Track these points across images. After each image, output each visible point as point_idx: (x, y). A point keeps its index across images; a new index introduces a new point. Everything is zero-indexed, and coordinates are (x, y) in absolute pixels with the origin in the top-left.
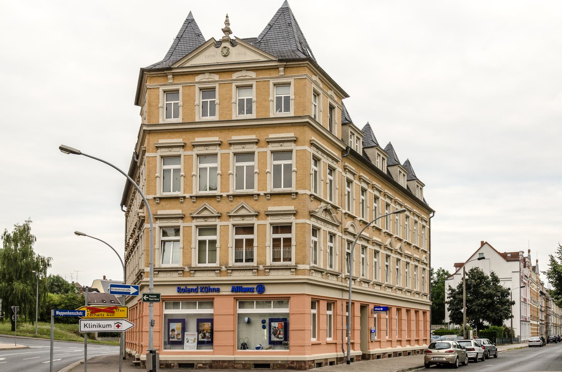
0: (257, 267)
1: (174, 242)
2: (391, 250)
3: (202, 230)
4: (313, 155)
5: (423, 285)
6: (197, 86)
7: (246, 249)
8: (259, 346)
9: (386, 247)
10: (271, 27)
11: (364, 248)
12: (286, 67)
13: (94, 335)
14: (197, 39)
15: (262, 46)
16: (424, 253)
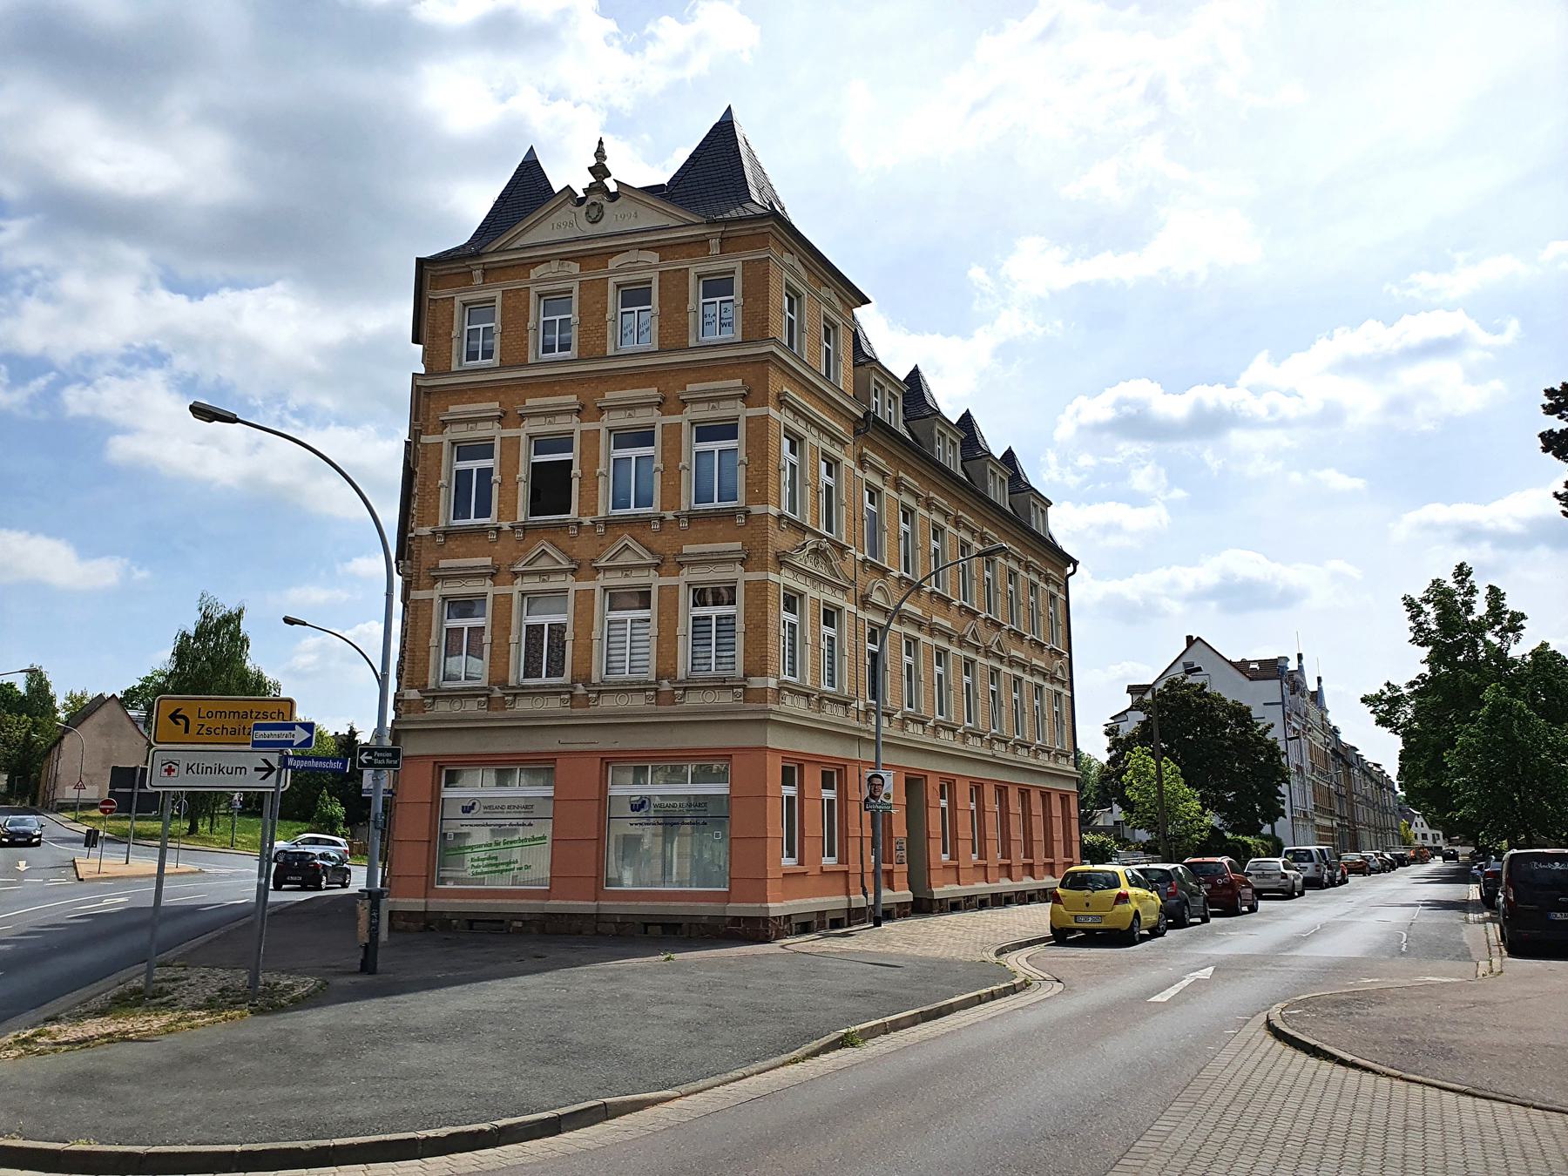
2: (977, 648)
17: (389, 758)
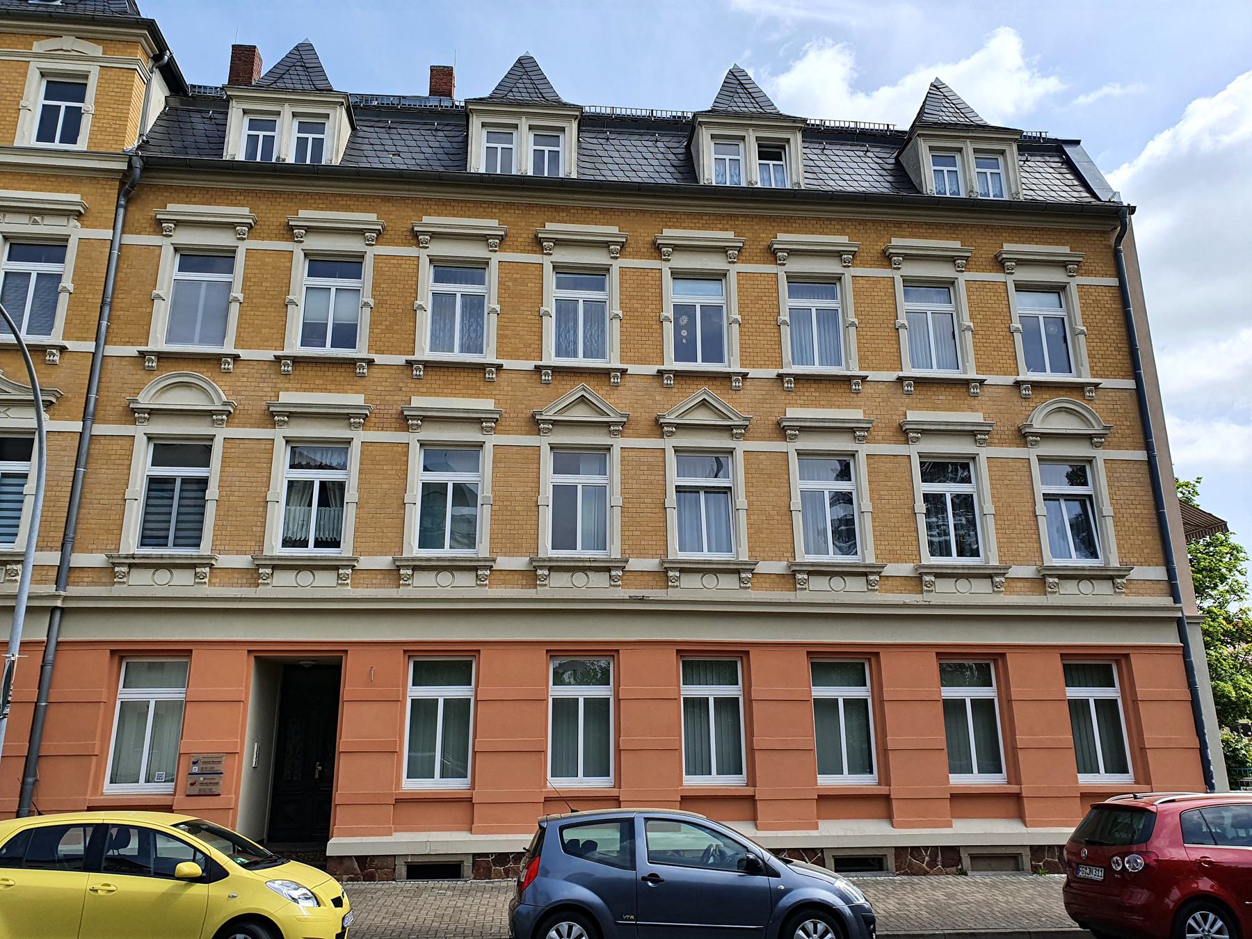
3: (567, 459)
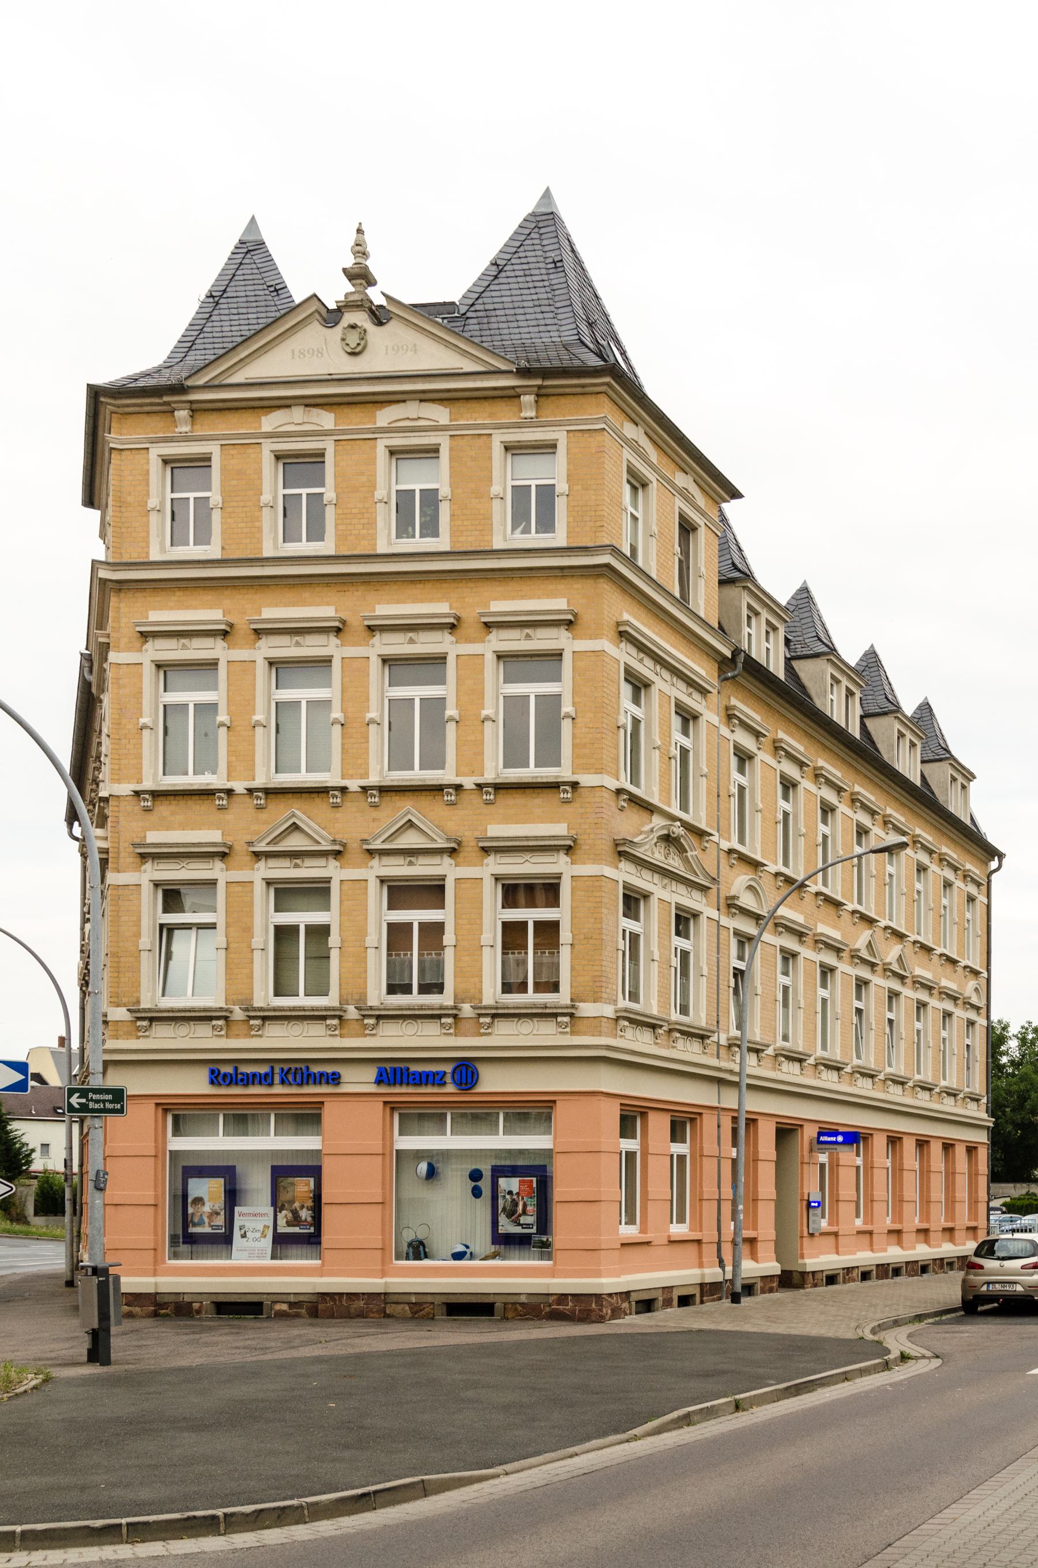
0: (455, 1008)
1: (200, 931)
2: (873, 965)
4: (625, 669)
5: (968, 1068)
6: (268, 447)
7: (420, 955)
8: (460, 1248)
9: (855, 957)
10: (500, 271)
11: (788, 956)
12: (541, 395)
13: (23, 1210)
14: (272, 303)
15: (471, 327)
16: (972, 975)
17: (108, 1101)
